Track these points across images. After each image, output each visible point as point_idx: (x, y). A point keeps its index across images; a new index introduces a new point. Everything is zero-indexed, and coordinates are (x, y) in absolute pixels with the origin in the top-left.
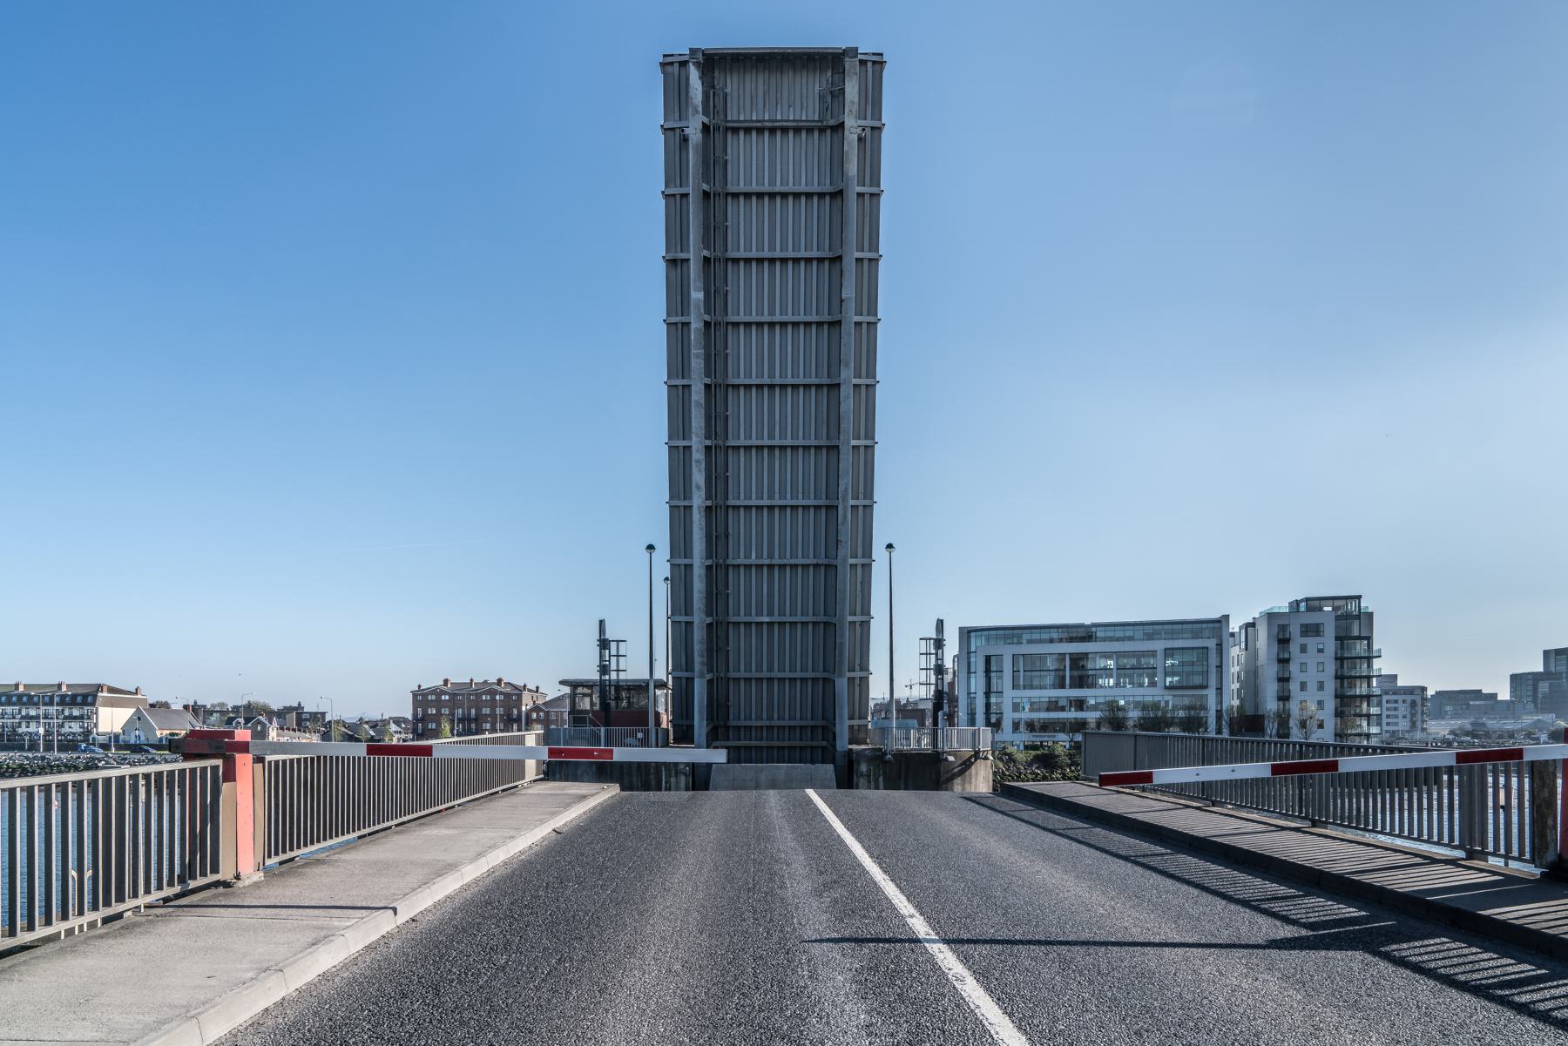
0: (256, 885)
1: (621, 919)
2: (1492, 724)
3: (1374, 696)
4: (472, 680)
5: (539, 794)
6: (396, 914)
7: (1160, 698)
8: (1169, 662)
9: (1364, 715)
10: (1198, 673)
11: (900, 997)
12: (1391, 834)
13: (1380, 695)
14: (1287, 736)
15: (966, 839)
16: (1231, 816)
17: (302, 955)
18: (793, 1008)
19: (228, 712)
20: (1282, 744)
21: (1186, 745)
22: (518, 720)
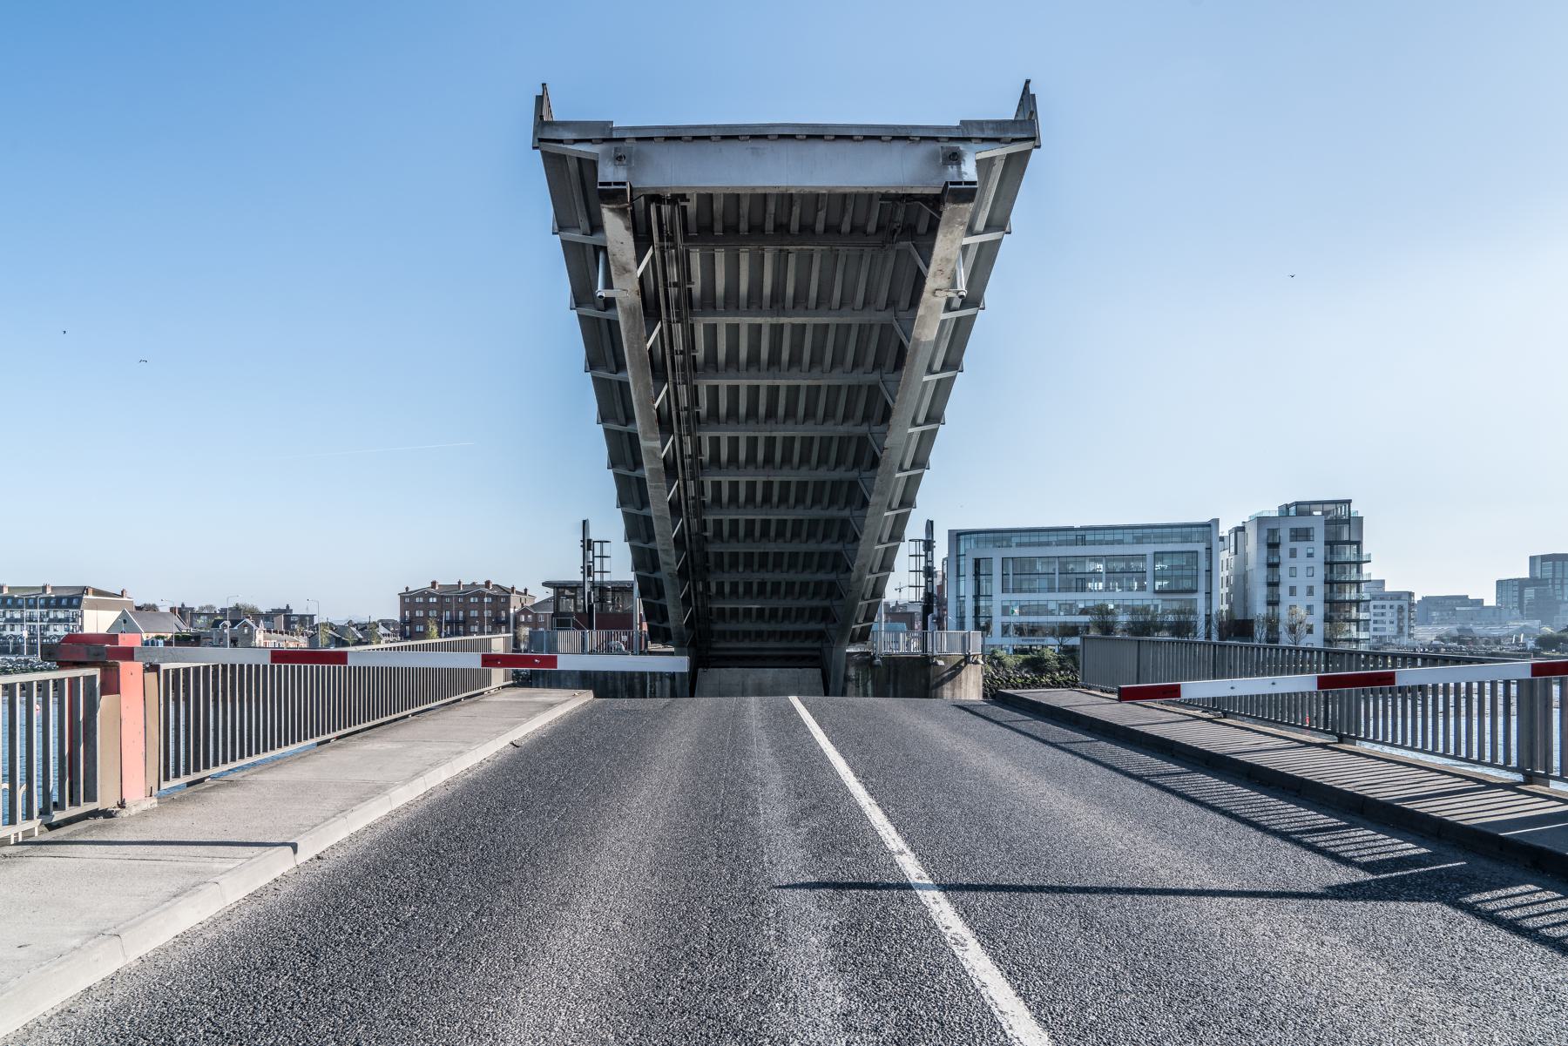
0: (145, 814)
1: (563, 855)
2: (1479, 630)
3: (1364, 601)
4: (460, 583)
5: (504, 702)
6: (295, 851)
7: (1149, 602)
8: (1158, 566)
9: (1353, 621)
10: (1187, 577)
11: (888, 971)
12: (1374, 741)
13: (1370, 601)
14: (1277, 641)
15: (960, 754)
16: (1248, 729)
17: (156, 910)
18: (752, 985)
19: (215, 614)
20: (1271, 649)
21: (1195, 652)
22: (506, 623)
